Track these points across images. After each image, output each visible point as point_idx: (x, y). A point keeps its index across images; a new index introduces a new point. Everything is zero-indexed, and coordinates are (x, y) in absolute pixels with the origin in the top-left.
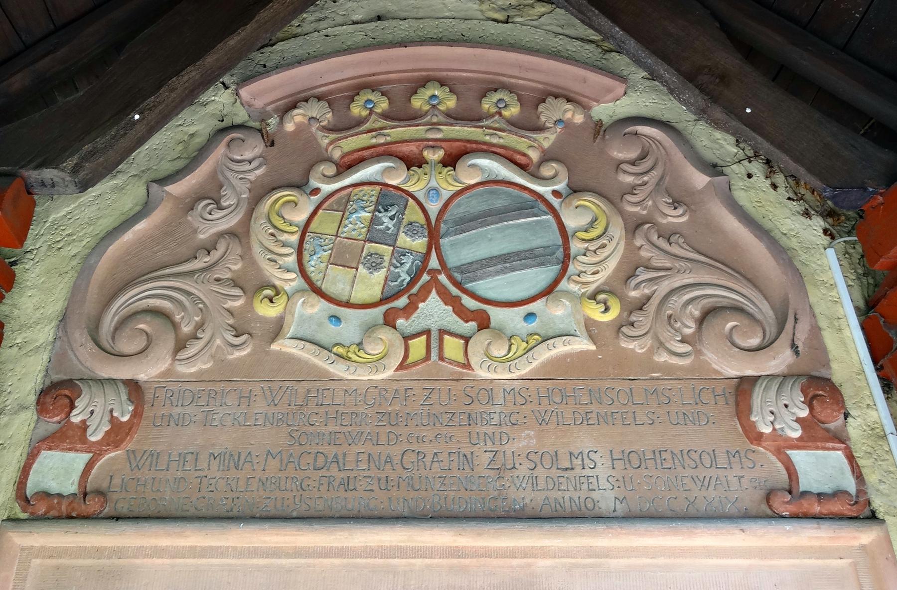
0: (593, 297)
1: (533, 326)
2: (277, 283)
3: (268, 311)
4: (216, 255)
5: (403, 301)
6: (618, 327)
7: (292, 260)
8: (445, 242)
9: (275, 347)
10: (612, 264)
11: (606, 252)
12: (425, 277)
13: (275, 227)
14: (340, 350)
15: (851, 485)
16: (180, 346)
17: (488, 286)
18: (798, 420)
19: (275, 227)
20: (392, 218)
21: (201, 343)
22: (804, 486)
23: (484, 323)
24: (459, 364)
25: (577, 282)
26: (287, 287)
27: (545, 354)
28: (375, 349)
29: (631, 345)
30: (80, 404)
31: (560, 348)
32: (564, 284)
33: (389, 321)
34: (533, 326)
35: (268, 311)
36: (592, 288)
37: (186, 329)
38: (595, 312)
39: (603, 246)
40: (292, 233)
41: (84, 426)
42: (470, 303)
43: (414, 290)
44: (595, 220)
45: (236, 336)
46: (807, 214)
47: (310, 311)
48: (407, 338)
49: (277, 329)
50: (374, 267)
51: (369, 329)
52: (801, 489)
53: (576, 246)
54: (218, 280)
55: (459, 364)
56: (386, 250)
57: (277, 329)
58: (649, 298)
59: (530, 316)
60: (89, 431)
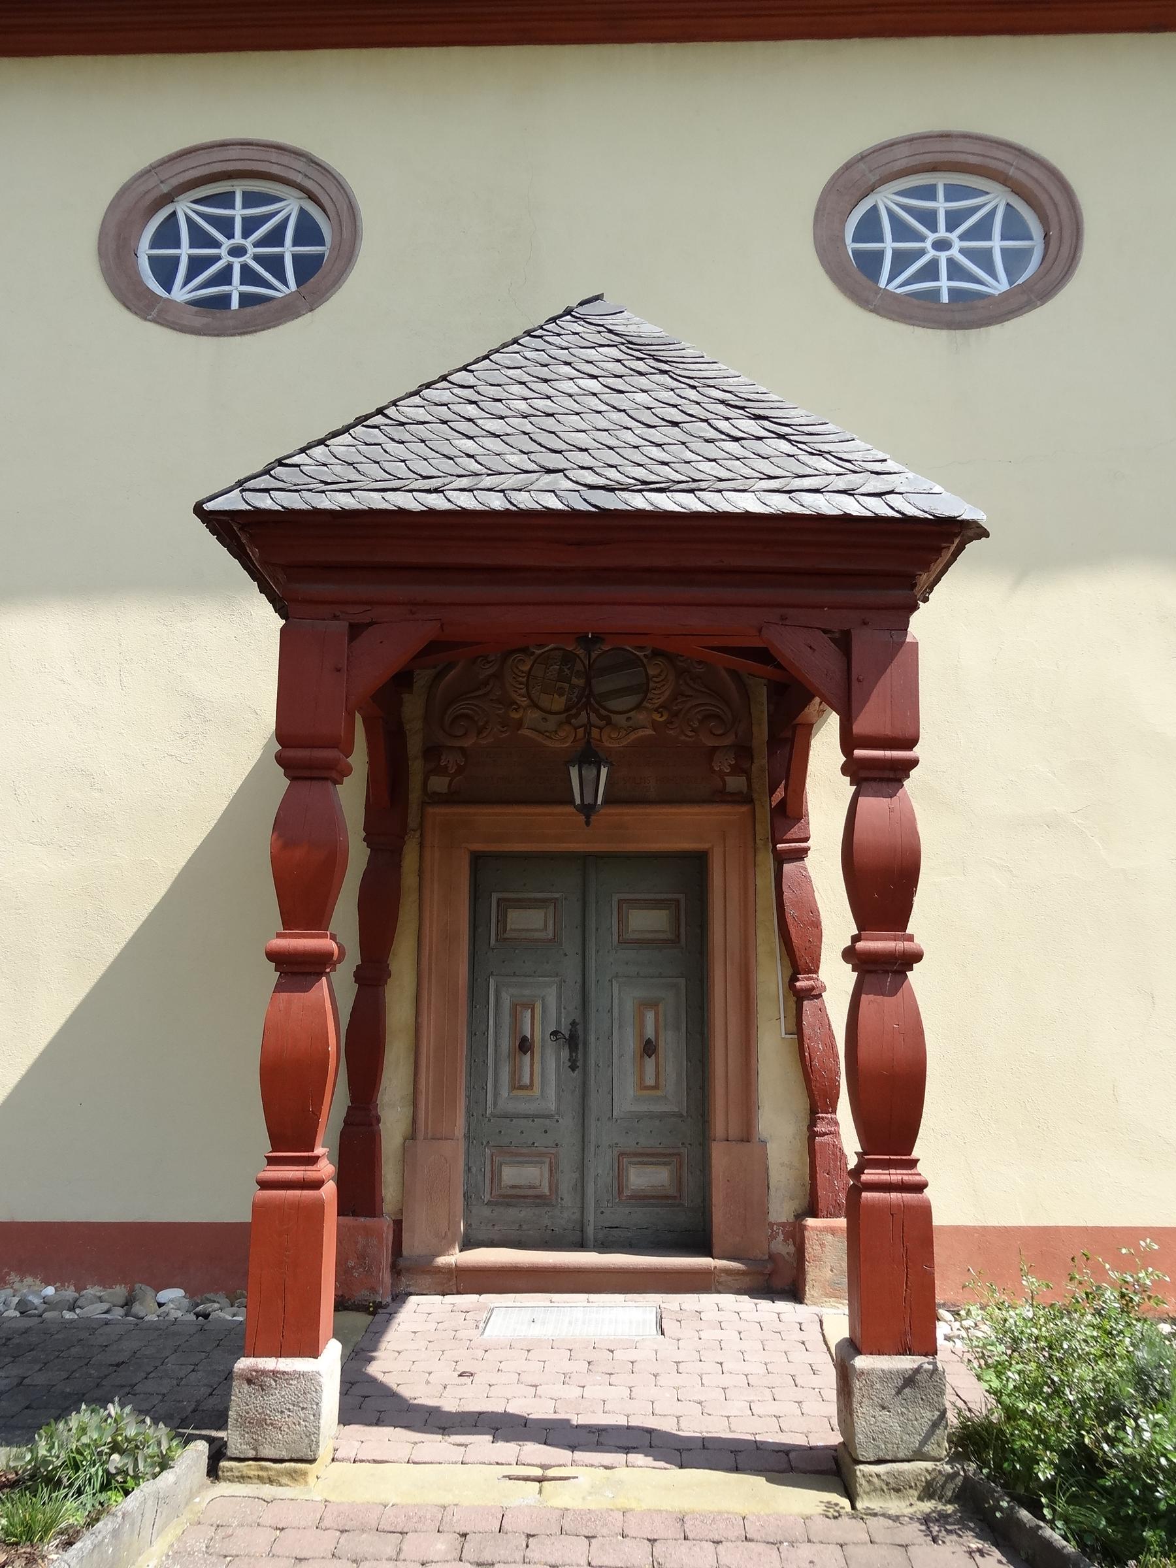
0: (656, 710)
1: (630, 723)
2: (519, 702)
3: (516, 716)
4: (489, 688)
5: (574, 711)
6: (669, 722)
7: (524, 691)
8: (593, 681)
9: (519, 732)
10: (667, 694)
11: (665, 687)
12: (584, 700)
13: (516, 674)
14: (548, 734)
15: (745, 790)
16: (479, 733)
17: (614, 704)
18: (730, 765)
19: (516, 674)
20: (569, 669)
21: (489, 730)
22: (727, 790)
23: (609, 722)
24: (598, 740)
25: (650, 703)
26: (524, 704)
27: (633, 736)
28: (562, 734)
29: (671, 732)
30: (443, 757)
31: (641, 733)
32: (645, 704)
33: (568, 722)
34: (630, 723)
35: (516, 716)
36: (656, 706)
37: (481, 724)
38: (657, 717)
39: (664, 685)
40: (524, 677)
41: (446, 767)
42: (603, 712)
43: (579, 706)
44: (661, 671)
45: (503, 727)
46: (715, 1267)
47: (534, 716)
48: (576, 728)
49: (520, 724)
50: (561, 695)
51: (560, 724)
52: (669, 1167)
53: (652, 685)
54: (491, 700)
55: (598, 740)
56: (567, 686)
57: (520, 724)
58: (681, 709)
59: (629, 719)
60: (449, 769)
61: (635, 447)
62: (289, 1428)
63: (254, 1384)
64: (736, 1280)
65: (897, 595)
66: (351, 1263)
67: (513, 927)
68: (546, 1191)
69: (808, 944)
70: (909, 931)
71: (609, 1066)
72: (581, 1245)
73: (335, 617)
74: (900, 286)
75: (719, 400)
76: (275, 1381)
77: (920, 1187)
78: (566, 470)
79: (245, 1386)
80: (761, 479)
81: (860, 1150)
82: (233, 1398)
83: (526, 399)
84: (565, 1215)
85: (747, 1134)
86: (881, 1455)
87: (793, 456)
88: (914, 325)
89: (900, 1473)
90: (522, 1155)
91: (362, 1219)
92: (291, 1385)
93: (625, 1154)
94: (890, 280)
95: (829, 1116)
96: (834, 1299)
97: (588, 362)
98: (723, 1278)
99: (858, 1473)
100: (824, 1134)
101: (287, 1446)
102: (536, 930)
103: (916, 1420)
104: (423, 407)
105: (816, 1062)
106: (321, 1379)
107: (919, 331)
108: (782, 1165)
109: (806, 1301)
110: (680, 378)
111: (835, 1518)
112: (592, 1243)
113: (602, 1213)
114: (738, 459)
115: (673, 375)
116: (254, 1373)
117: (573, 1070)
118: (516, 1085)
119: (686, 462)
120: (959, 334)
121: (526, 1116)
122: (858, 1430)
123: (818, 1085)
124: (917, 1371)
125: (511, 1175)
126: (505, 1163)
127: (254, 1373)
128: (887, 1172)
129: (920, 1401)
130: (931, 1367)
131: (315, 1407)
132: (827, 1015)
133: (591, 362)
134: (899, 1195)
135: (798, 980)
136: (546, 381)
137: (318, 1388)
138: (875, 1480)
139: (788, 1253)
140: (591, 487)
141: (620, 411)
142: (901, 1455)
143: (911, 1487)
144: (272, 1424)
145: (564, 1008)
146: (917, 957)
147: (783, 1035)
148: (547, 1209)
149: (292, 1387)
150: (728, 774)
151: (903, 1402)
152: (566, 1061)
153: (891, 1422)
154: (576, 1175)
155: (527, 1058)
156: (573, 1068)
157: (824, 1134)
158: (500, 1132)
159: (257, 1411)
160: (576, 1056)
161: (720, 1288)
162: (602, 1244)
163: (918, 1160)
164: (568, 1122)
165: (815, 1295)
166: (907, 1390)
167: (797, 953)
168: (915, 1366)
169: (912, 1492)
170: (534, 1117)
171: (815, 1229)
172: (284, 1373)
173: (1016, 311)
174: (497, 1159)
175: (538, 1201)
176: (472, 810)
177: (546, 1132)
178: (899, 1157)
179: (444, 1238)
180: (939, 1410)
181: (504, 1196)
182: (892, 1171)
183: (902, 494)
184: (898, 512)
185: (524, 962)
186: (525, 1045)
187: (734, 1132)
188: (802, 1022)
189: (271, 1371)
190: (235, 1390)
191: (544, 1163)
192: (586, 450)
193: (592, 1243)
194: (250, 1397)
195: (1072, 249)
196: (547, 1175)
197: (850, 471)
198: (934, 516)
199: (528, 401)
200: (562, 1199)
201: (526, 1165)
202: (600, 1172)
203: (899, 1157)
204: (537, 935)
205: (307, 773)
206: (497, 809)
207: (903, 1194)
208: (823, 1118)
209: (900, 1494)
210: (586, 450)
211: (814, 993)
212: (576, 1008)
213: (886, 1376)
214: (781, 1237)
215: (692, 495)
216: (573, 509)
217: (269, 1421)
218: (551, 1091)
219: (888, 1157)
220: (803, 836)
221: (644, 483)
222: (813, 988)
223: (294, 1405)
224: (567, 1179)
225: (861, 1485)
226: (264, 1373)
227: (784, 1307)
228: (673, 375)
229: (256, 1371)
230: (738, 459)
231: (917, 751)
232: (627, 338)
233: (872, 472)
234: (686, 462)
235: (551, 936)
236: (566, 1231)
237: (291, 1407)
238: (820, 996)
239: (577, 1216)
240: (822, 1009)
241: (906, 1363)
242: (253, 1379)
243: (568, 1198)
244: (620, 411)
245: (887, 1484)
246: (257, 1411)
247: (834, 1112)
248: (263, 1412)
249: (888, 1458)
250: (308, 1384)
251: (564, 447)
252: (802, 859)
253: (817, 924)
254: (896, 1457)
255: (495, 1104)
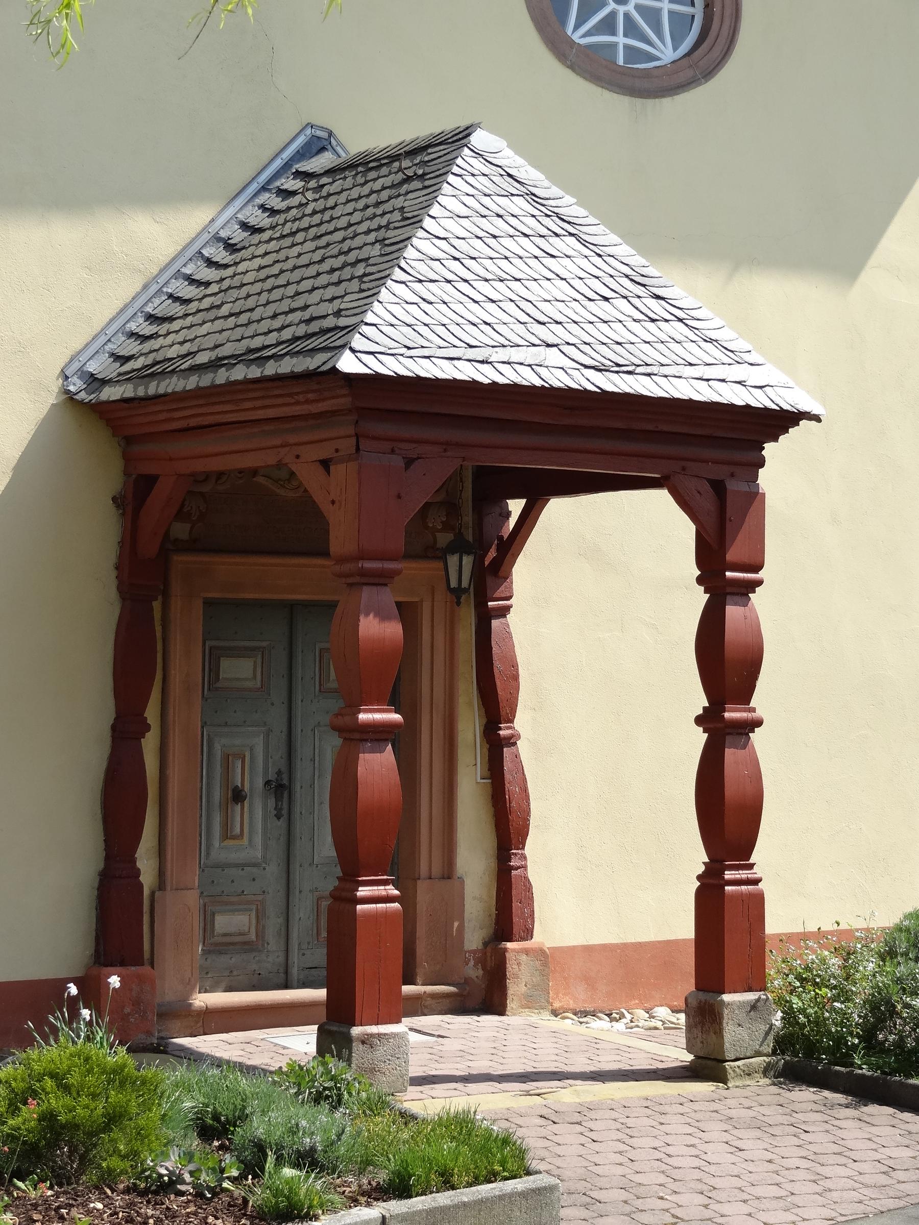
61: (590, 322)
62: (390, 1072)
63: (366, 1044)
64: (439, 1003)
65: (749, 456)
66: (127, 1010)
67: (225, 676)
68: (253, 937)
69: (509, 696)
70: (752, 704)
71: (311, 813)
72: (286, 986)
73: (393, 451)
74: (584, 36)
75: (624, 274)
76: (380, 1041)
77: (756, 882)
78: (526, 323)
79: (361, 1046)
80: (685, 365)
81: (707, 860)
82: (353, 1054)
83: (491, 259)
84: (270, 959)
85: (448, 872)
86: (738, 1055)
87: (694, 342)
88: (602, 87)
89: (751, 1063)
90: (232, 903)
91: (133, 968)
92: (390, 1042)
93: (323, 898)
94: (576, 27)
95: (520, 851)
96: (527, 1010)
97: (513, 215)
98: (429, 1001)
99: (727, 1066)
100: (519, 868)
101: (389, 1085)
102: (246, 679)
103: (757, 1031)
104: (423, 260)
105: (514, 804)
106: (409, 1037)
107: (608, 95)
108: (474, 898)
109: (507, 1013)
110: (587, 244)
111: (727, 1089)
112: (295, 983)
113: (304, 954)
114: (662, 342)
115: (578, 237)
116: (366, 1036)
117: (279, 818)
118: (227, 835)
119: (631, 343)
120: (638, 102)
121: (237, 866)
122: (726, 1040)
123: (514, 824)
124: (758, 1000)
125: (224, 923)
126: (219, 912)
127: (366, 1036)
128: (737, 872)
129: (759, 1019)
130: (765, 997)
131: (405, 1056)
132: (521, 761)
133: (516, 216)
134: (746, 887)
135: (500, 729)
136: (495, 237)
137: (407, 1043)
138: (737, 1070)
139: (477, 977)
140: (586, 367)
141: (562, 279)
142: (748, 1054)
143: (756, 1072)
144: (379, 1071)
145: (271, 758)
146: (759, 723)
147: (479, 780)
148: (255, 954)
149: (390, 1044)
150: (439, 531)
151: (750, 1020)
152: (272, 810)
153: (743, 1033)
154: (281, 920)
155: (238, 808)
156: (278, 817)
157: (519, 868)
158: (213, 882)
159: (369, 1062)
160: (282, 804)
161: (426, 1011)
162: (303, 984)
163: (755, 864)
164: (273, 870)
165: (514, 1007)
166: (752, 1013)
167: (501, 704)
168: (757, 997)
169: (756, 1075)
170: (242, 866)
171: (514, 950)
172: (385, 1034)
173: (684, 86)
174: (209, 908)
175: (246, 947)
176: (205, 558)
177: (254, 880)
178: (745, 862)
179: (188, 984)
180: (769, 1024)
181: (216, 944)
182: (741, 872)
183: (772, 386)
184: (777, 405)
185: (235, 712)
186: (238, 796)
187: (436, 870)
188: (503, 767)
189: (376, 1034)
190: (354, 1049)
191: (251, 910)
192: (560, 323)
193: (295, 983)
194: (364, 1053)
195: (731, 31)
196: (254, 921)
197: (736, 361)
198: (798, 410)
199: (494, 260)
200: (268, 944)
201: (236, 913)
202: (302, 915)
203: (745, 862)
204: (249, 684)
205: (376, 580)
206: (238, 559)
207: (749, 887)
208: (515, 854)
209: (751, 1077)
210: (560, 323)
211: (512, 741)
212: (282, 757)
213: (742, 1005)
214: (472, 963)
215: (649, 378)
216: (585, 389)
217: (377, 1069)
218: (258, 840)
219: (738, 863)
220: (508, 595)
221: (618, 365)
222: (512, 736)
223: (392, 1056)
224: (274, 923)
225: (730, 1074)
226: (372, 1035)
227: (489, 1021)
228: (578, 237)
229: (367, 1035)
230: (662, 342)
231: (761, 575)
232: (530, 188)
233: (749, 364)
234: (631, 343)
235: (259, 685)
236: (271, 974)
237: (390, 1058)
238: (515, 744)
239: (282, 959)
240: (517, 756)
241: (751, 996)
242: (366, 1040)
243: (274, 943)
244: (562, 279)
245: (744, 1071)
246: (369, 1062)
247: (523, 848)
248: (373, 1063)
249: (742, 1057)
250: (400, 1040)
251: (546, 319)
252: (504, 616)
253: (516, 678)
254: (746, 1056)
255: (208, 854)
